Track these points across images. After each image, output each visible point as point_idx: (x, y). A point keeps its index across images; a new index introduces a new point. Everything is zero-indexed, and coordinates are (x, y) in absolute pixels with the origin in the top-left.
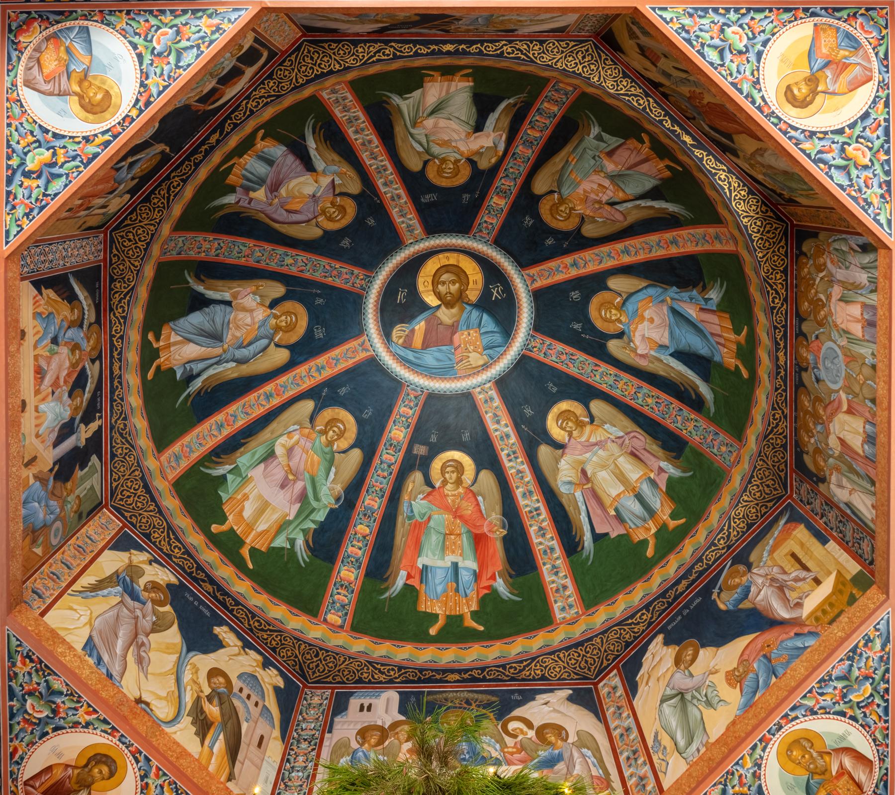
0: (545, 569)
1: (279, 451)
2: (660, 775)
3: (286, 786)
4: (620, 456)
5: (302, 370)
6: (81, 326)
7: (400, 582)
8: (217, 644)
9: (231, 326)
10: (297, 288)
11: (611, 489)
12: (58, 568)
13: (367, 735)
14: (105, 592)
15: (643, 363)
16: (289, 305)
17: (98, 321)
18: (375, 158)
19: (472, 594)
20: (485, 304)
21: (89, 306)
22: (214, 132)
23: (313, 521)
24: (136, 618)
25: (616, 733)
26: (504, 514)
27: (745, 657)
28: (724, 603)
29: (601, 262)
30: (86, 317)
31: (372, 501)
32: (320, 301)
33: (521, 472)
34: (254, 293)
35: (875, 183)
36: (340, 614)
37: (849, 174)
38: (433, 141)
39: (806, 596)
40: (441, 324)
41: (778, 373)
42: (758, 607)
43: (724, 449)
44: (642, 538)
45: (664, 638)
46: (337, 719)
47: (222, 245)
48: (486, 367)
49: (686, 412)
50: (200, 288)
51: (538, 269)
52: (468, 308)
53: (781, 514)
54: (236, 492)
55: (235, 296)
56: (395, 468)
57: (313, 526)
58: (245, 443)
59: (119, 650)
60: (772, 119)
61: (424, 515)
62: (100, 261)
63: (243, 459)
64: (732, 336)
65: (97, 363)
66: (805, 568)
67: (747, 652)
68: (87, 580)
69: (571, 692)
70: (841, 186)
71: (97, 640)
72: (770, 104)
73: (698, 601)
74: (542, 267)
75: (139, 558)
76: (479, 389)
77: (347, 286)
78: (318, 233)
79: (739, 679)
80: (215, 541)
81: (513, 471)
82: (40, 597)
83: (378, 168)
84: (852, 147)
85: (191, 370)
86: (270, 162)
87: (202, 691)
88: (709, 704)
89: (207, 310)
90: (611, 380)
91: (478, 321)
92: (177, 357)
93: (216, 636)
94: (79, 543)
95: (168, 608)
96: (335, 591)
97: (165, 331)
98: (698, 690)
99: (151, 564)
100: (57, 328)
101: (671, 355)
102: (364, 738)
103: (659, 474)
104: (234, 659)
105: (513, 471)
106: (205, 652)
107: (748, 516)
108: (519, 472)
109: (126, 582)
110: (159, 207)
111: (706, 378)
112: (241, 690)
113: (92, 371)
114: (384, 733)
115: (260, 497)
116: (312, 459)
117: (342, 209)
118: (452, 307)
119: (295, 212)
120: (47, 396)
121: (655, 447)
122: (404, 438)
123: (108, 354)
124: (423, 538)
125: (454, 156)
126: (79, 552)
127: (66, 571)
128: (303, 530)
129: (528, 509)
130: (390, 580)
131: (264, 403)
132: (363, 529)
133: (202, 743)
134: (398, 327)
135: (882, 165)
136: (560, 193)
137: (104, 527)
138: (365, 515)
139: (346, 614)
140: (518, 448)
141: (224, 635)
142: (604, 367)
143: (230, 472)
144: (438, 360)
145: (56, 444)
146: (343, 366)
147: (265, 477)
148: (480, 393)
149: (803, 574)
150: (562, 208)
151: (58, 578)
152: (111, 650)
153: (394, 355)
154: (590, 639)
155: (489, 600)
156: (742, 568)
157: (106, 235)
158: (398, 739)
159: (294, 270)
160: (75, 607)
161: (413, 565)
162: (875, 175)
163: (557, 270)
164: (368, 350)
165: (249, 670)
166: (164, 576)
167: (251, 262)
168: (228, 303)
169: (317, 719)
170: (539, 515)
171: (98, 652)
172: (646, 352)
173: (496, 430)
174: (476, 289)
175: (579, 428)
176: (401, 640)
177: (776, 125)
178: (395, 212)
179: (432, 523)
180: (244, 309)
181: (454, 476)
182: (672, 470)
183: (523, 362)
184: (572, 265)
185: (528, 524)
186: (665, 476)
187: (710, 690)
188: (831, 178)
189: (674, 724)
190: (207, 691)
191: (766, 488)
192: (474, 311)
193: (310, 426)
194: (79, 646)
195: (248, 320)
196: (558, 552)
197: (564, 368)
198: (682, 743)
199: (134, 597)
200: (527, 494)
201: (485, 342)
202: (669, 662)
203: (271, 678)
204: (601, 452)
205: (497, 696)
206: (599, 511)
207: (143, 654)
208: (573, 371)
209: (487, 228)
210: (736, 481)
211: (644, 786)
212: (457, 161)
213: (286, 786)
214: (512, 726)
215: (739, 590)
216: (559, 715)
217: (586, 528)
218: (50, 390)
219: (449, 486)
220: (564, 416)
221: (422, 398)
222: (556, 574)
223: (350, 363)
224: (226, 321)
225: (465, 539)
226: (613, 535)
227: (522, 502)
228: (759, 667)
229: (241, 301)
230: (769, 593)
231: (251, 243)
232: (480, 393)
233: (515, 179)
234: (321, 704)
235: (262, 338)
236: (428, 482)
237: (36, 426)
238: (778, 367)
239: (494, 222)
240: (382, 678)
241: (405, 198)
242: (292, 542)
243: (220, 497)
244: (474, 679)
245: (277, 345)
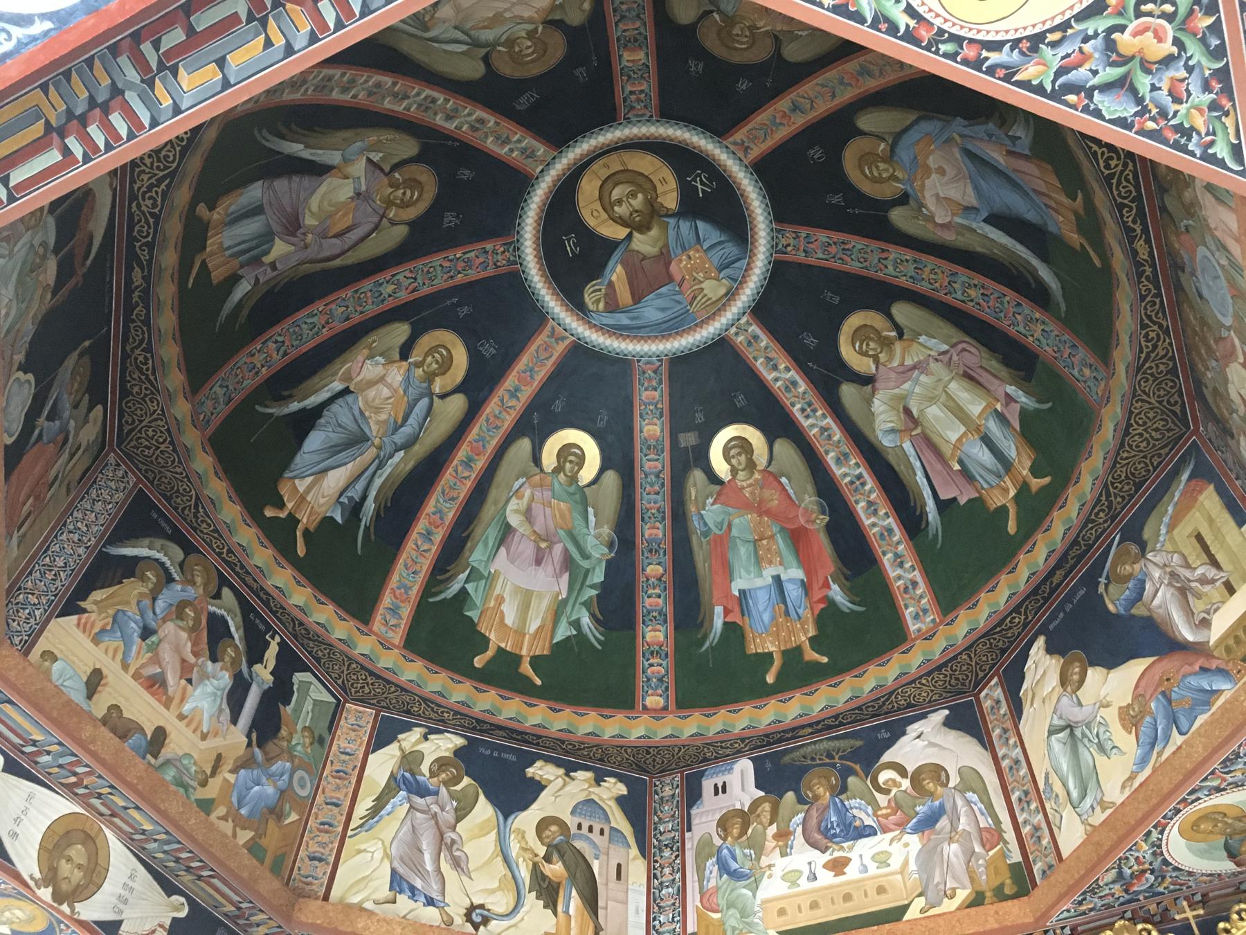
0: (887, 560)
1: (514, 520)
2: (1055, 830)
3: (660, 907)
4: (950, 381)
5: (492, 407)
6: (170, 579)
7: (718, 622)
8: (537, 788)
9: (367, 414)
10: (422, 315)
11: (952, 432)
12: (326, 814)
13: (729, 824)
14: (389, 807)
15: (949, 237)
16: (427, 340)
17: (188, 548)
18: (406, 97)
19: (806, 614)
20: (691, 207)
21: (162, 549)
22: (130, 269)
23: (592, 587)
24: (435, 816)
25: (1005, 764)
26: (820, 493)
27: (1140, 691)
28: (1113, 602)
29: (834, 96)
30: (168, 564)
31: (653, 530)
32: (464, 311)
33: (826, 430)
34: (370, 357)
35: (1195, 85)
36: (660, 691)
37: (1133, 91)
38: (473, 28)
39: (1216, 610)
40: (645, 258)
41: (1140, 275)
42: (1155, 616)
43: (1087, 372)
44: (999, 504)
45: (1046, 642)
46: (694, 811)
47: (280, 339)
48: (731, 295)
49: (1027, 308)
50: (295, 406)
51: (745, 130)
52: (672, 221)
53: (1183, 461)
54: (486, 599)
55: (348, 378)
56: (666, 475)
57: (594, 592)
58: (468, 536)
59: (429, 866)
60: (943, 48)
61: (722, 523)
62: (135, 485)
63: (476, 556)
64: (1065, 200)
65: (226, 592)
66: (1215, 563)
67: (1143, 684)
68: (364, 805)
69: (947, 712)
70: (1122, 123)
71: (401, 870)
72: (927, 16)
73: (1082, 592)
74: (750, 126)
75: (410, 739)
76: (733, 330)
77: (490, 272)
78: (402, 231)
79: (1134, 721)
80: (486, 678)
81: (815, 430)
82: (320, 860)
83: (420, 105)
84: (1128, 31)
85: (351, 499)
86: (256, 211)
87: (536, 855)
88: (1101, 748)
89: (322, 421)
90: (910, 269)
91: (693, 235)
92: (322, 501)
93: (532, 779)
94: (337, 767)
95: (466, 781)
96: (646, 664)
97: (284, 490)
98: (1088, 726)
99: (427, 739)
100: (138, 617)
101: (985, 221)
102: (725, 830)
103: (1007, 405)
104: (561, 793)
105: (815, 430)
106: (525, 807)
107: (1133, 474)
108: (823, 429)
109: (407, 781)
110: (146, 395)
111: (1044, 258)
112: (580, 827)
113: (227, 607)
114: (744, 817)
115: (517, 589)
116: (560, 510)
117: (413, 183)
118: (649, 229)
119: (349, 230)
120: (184, 690)
121: (994, 363)
122: (662, 431)
123: (231, 575)
124: (730, 556)
125: (521, 30)
126: (340, 778)
127: (336, 810)
128: (584, 604)
129: (847, 479)
130: (706, 624)
131: (466, 474)
132: (654, 569)
133: (555, 913)
134: (588, 289)
135: (1203, 41)
136: (719, 11)
137: (355, 728)
138: (651, 551)
139: (667, 688)
140: (811, 396)
141: (540, 772)
142: (895, 252)
143: (467, 581)
144: (663, 310)
145: (234, 721)
146: (541, 375)
147: (512, 563)
148: (737, 334)
149: (1212, 572)
150: (736, 31)
151: (330, 825)
152: (422, 873)
153: (601, 329)
154: (955, 657)
155: (828, 616)
156: (1134, 548)
157: (114, 452)
158: (761, 823)
159: (403, 296)
160: (362, 847)
161: (728, 594)
162: (1190, 70)
163: (774, 123)
164: (564, 338)
165: (582, 797)
166: (446, 744)
167: (339, 326)
168: (346, 391)
169: (673, 816)
170: (863, 484)
171: (408, 882)
172: (948, 219)
173: (776, 380)
174: (671, 191)
175: (885, 349)
176: (736, 701)
177: (952, 56)
178: (490, 144)
179: (734, 532)
180: (371, 383)
181: (743, 458)
182: (1023, 398)
183: (779, 271)
184: (794, 110)
185: (853, 499)
186: (1016, 408)
187: (1102, 729)
188: (1098, 114)
189: (1065, 767)
190: (542, 850)
191: (1153, 433)
192: (681, 222)
193: (538, 470)
194: (385, 892)
195: (386, 392)
196: (898, 535)
197: (838, 265)
198: (1075, 794)
199: (423, 792)
200: (842, 459)
201: (716, 260)
202: (1053, 680)
203: (614, 788)
204: (923, 378)
205: (861, 738)
206: (939, 467)
207: (457, 853)
208: (853, 266)
209: (639, 100)
210: (1107, 434)
211: (1039, 838)
212: (531, 35)
213: (660, 907)
214: (885, 776)
215: (1130, 585)
216: (935, 750)
217: (927, 493)
218: (183, 682)
219: (741, 475)
220: (861, 334)
221: (664, 370)
222: (901, 565)
223: (550, 364)
224: (357, 413)
225: (780, 540)
226: (963, 500)
227: (838, 471)
228: (1157, 708)
229: (359, 378)
230: (1168, 596)
231: (319, 306)
232: (737, 334)
233: (638, 16)
234: (673, 795)
235: (416, 401)
236: (713, 478)
237: (194, 731)
238: (1138, 264)
239: (644, 87)
240: (728, 751)
241: (491, 120)
242: (576, 624)
243: (470, 619)
244: (829, 728)
245: (443, 396)
